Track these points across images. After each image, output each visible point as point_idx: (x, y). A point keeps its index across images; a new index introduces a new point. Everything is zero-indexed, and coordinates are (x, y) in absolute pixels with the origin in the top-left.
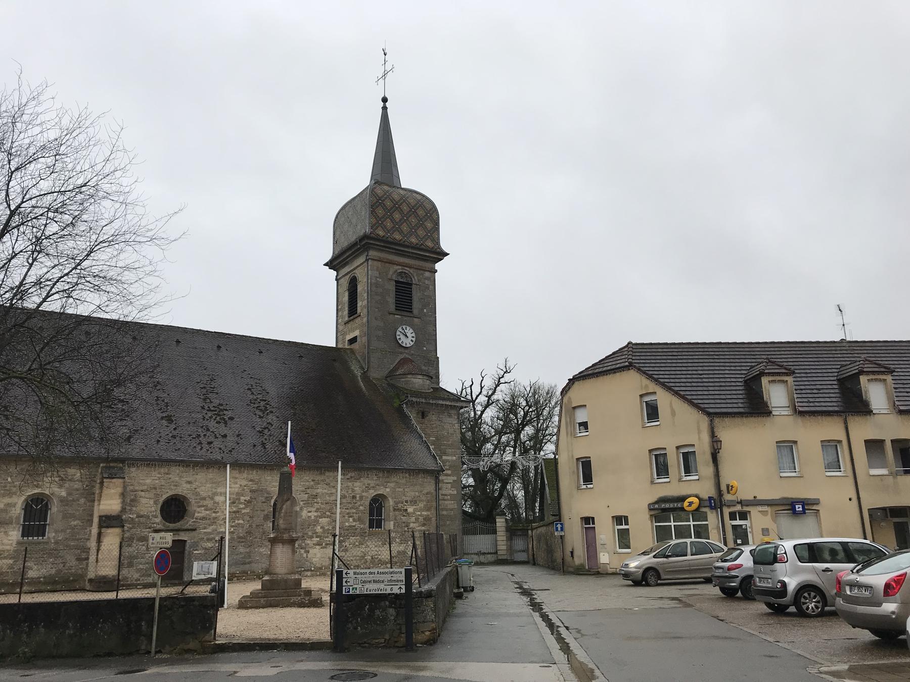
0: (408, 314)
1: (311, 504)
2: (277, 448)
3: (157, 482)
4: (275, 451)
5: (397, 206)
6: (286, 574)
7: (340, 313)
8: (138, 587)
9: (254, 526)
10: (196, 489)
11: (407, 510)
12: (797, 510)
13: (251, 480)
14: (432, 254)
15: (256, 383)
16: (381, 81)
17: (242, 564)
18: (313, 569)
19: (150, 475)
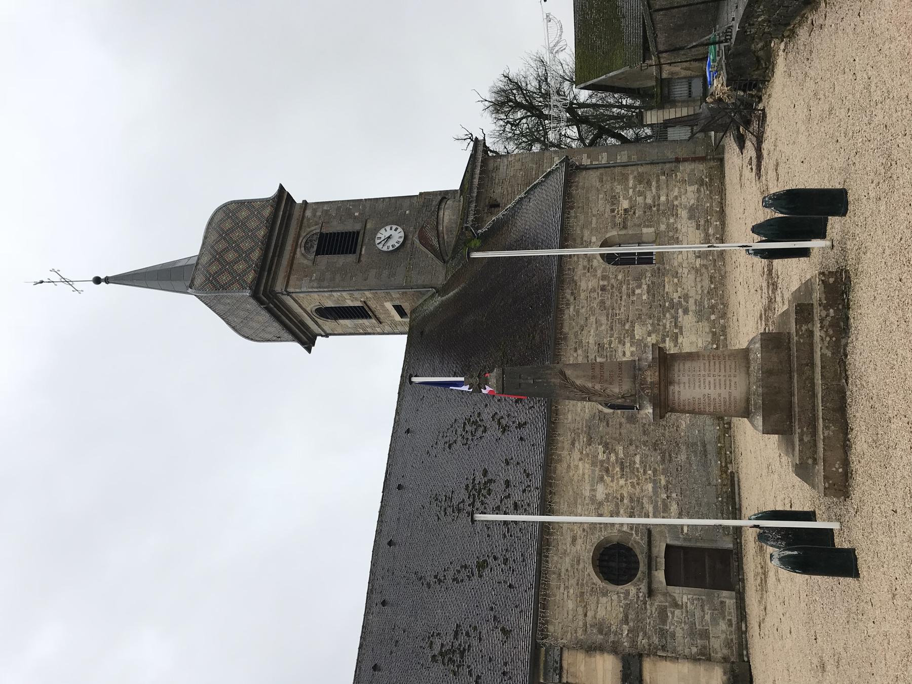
1: (612, 351)
2: (526, 406)
3: (571, 591)
4: (530, 408)
6: (748, 374)
7: (369, 330)
8: (744, 629)
9: (646, 438)
10: (584, 530)
11: (625, 210)
13: (573, 444)
14: (280, 206)
15: (443, 437)
16: (76, 285)
17: (706, 456)
18: (715, 346)
19: (562, 602)
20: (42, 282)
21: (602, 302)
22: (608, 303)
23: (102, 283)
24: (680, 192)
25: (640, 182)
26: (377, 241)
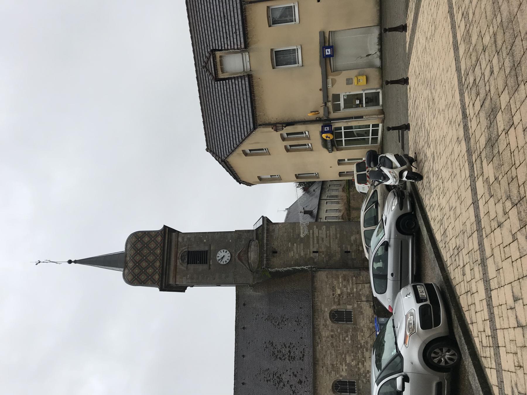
0: (208, 254)
5: (138, 252)
11: (339, 295)
12: (330, 54)
14: (166, 238)
21: (332, 343)
22: (335, 344)
23: (72, 263)
24: (362, 287)
25: (345, 280)
26: (218, 259)
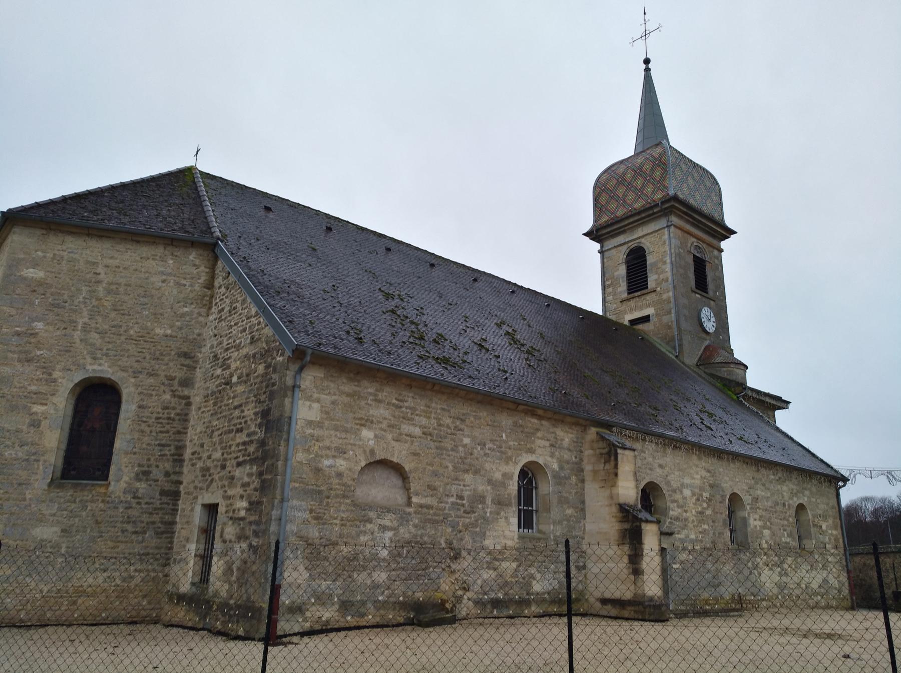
9: (717, 535)
20: (645, 14)
